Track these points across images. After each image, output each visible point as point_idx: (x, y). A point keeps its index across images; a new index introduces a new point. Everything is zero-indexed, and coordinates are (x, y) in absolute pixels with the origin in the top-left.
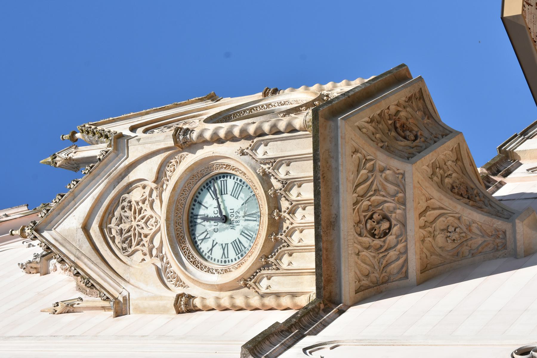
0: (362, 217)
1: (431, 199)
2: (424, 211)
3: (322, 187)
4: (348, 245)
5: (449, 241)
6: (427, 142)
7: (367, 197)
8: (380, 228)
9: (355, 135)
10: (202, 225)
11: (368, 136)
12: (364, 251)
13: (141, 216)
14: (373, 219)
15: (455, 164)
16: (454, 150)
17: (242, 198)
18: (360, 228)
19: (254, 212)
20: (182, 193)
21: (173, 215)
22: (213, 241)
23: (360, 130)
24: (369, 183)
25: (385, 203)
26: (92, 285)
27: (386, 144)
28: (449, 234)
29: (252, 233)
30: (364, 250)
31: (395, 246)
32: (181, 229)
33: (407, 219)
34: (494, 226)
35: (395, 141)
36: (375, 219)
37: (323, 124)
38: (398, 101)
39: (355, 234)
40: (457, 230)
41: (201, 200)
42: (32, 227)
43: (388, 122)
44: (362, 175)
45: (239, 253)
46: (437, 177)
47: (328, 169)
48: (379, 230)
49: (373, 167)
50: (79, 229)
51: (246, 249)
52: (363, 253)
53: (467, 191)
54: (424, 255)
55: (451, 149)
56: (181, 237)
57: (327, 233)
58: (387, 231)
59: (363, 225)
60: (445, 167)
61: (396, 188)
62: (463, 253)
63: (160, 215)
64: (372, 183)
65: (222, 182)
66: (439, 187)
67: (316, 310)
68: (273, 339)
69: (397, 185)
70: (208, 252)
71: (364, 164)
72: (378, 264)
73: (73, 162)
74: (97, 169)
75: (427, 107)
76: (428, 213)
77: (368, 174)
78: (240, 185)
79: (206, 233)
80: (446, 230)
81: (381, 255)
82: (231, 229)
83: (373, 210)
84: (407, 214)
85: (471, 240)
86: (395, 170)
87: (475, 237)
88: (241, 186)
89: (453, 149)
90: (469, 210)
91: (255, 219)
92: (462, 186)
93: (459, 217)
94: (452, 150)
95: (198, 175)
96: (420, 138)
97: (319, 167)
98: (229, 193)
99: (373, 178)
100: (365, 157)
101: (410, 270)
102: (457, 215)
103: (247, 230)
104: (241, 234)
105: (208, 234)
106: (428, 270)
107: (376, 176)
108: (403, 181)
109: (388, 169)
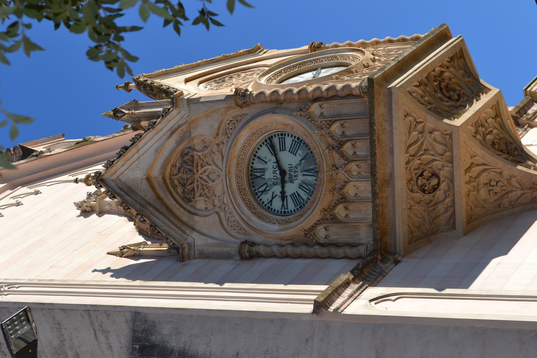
0: (413, 175)
1: (475, 156)
2: (469, 167)
3: (378, 149)
4: (402, 201)
5: (492, 194)
6: (469, 101)
7: (418, 156)
8: (429, 184)
9: (407, 100)
10: (262, 178)
11: (418, 99)
12: (415, 206)
13: (204, 168)
14: (423, 177)
15: (494, 120)
16: (494, 107)
17: (299, 155)
18: (412, 184)
19: (311, 168)
20: (242, 149)
21: (234, 169)
22: (273, 193)
23: (411, 94)
24: (419, 143)
25: (434, 161)
26: (159, 232)
27: (434, 105)
28: (491, 188)
29: (310, 187)
30: (416, 205)
31: (443, 200)
32: (242, 181)
33: (455, 176)
34: (533, 180)
35: (442, 102)
36: (425, 176)
37: (378, 90)
38: (442, 62)
39: (408, 191)
40: (499, 184)
41: (260, 156)
42: (98, 177)
43: (434, 84)
44: (413, 136)
45: (298, 205)
46: (480, 135)
47: (383, 132)
48: (429, 185)
49: (423, 129)
50: (143, 180)
51: (305, 201)
52: (415, 207)
53: (507, 146)
54: (469, 208)
55: (491, 107)
56: (243, 189)
57: (382, 191)
58: (436, 187)
59: (414, 182)
60: (486, 124)
61: (444, 148)
62: (504, 204)
63: (221, 168)
64: (422, 143)
65: (281, 139)
66: (482, 145)
67: (375, 261)
68: (340, 291)
69: (446, 145)
70: (268, 203)
71: (415, 126)
72: (428, 217)
73: (134, 116)
74: (160, 125)
75: (467, 66)
76: (473, 169)
77: (418, 135)
78: (298, 143)
79: (265, 186)
80: (488, 184)
81: (430, 209)
82: (290, 182)
83: (423, 168)
84: (455, 171)
85: (511, 193)
86: (443, 131)
87: (515, 190)
88: (299, 144)
89: (492, 106)
90: (510, 166)
91: (313, 174)
92: (502, 141)
93: (500, 172)
94: (492, 108)
95: (257, 133)
96: (463, 97)
97: (375, 131)
98: (288, 149)
99: (423, 139)
100: (415, 119)
101: (458, 222)
102: (498, 171)
103: (306, 184)
104: (299, 188)
105: (267, 186)
106: (473, 221)
107: (425, 137)
108: (451, 141)
109: (437, 131)
